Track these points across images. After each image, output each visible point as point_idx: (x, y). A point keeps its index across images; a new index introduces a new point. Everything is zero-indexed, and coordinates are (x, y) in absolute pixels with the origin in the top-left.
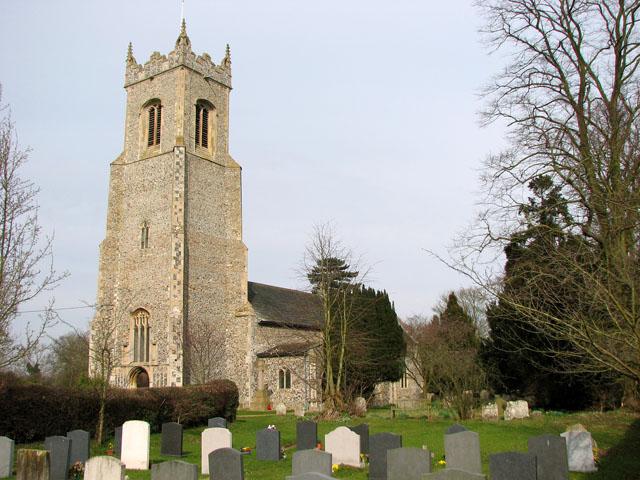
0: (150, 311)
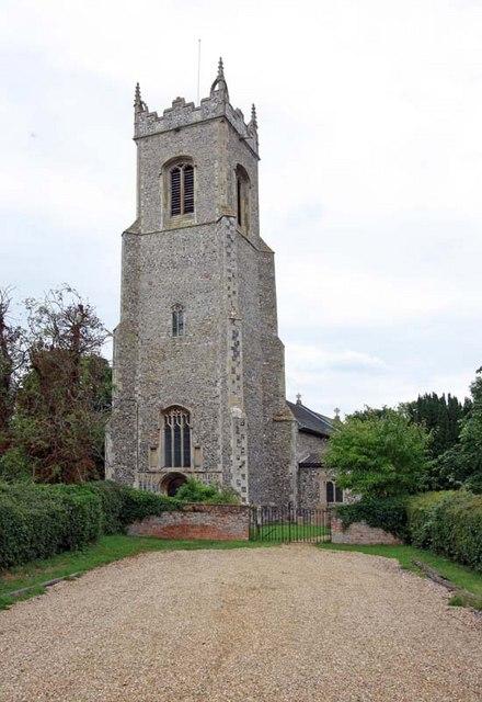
0: (190, 409)
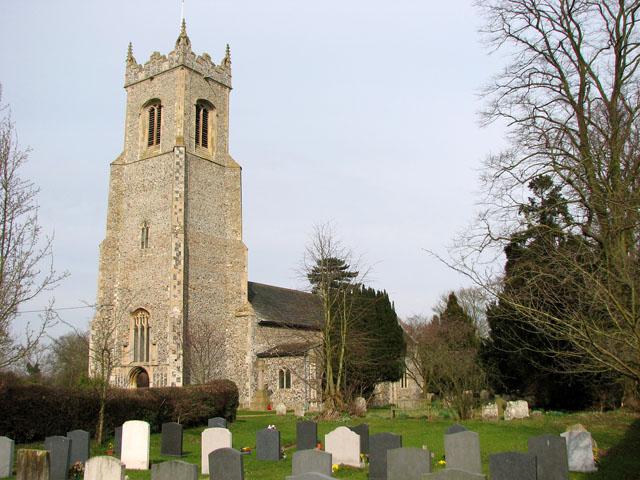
0: (150, 311)
